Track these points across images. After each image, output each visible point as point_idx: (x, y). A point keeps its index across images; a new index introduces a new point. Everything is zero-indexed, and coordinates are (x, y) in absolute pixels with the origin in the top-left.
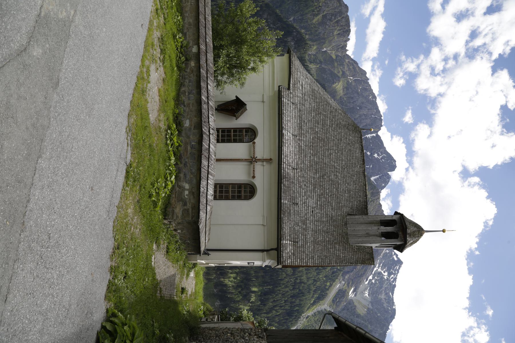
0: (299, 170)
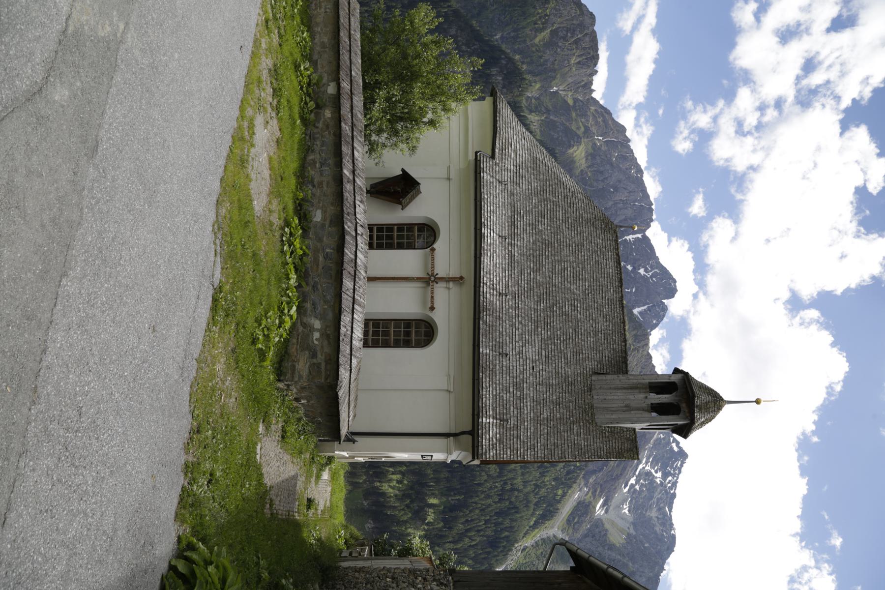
0: (510, 297)
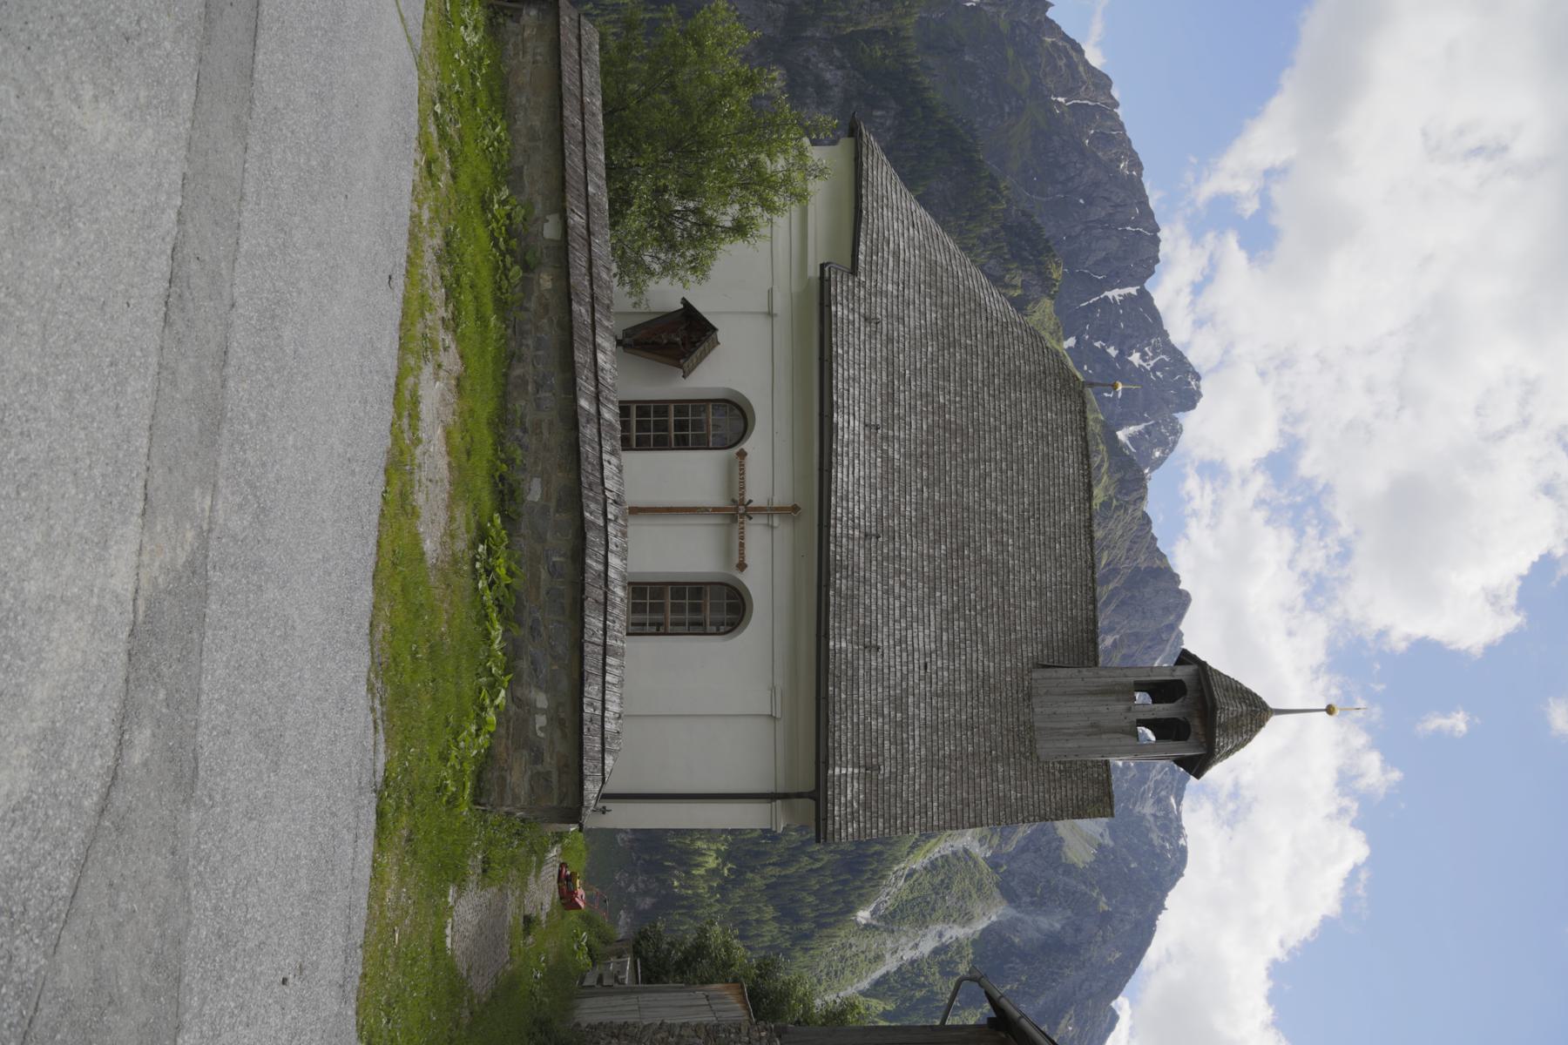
0: (885, 539)
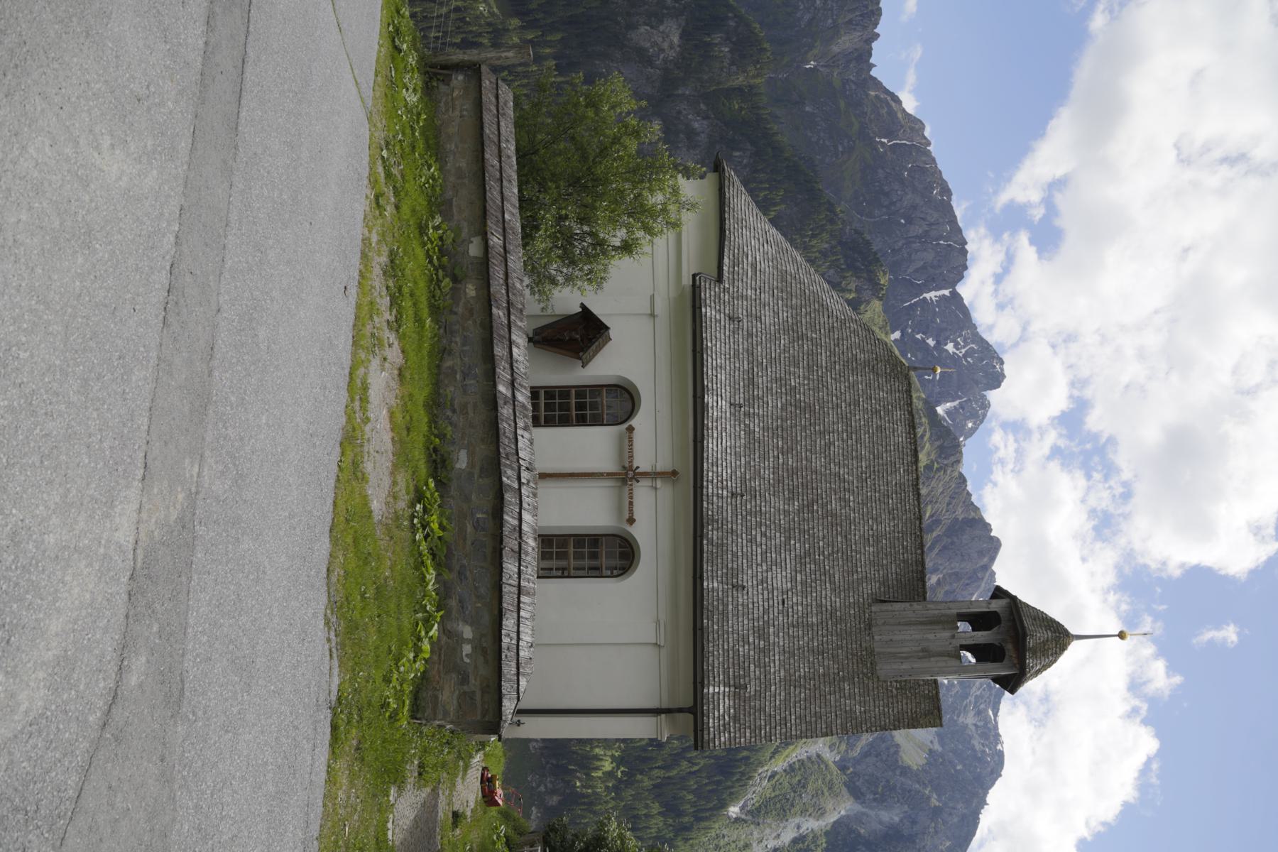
0: (749, 497)
